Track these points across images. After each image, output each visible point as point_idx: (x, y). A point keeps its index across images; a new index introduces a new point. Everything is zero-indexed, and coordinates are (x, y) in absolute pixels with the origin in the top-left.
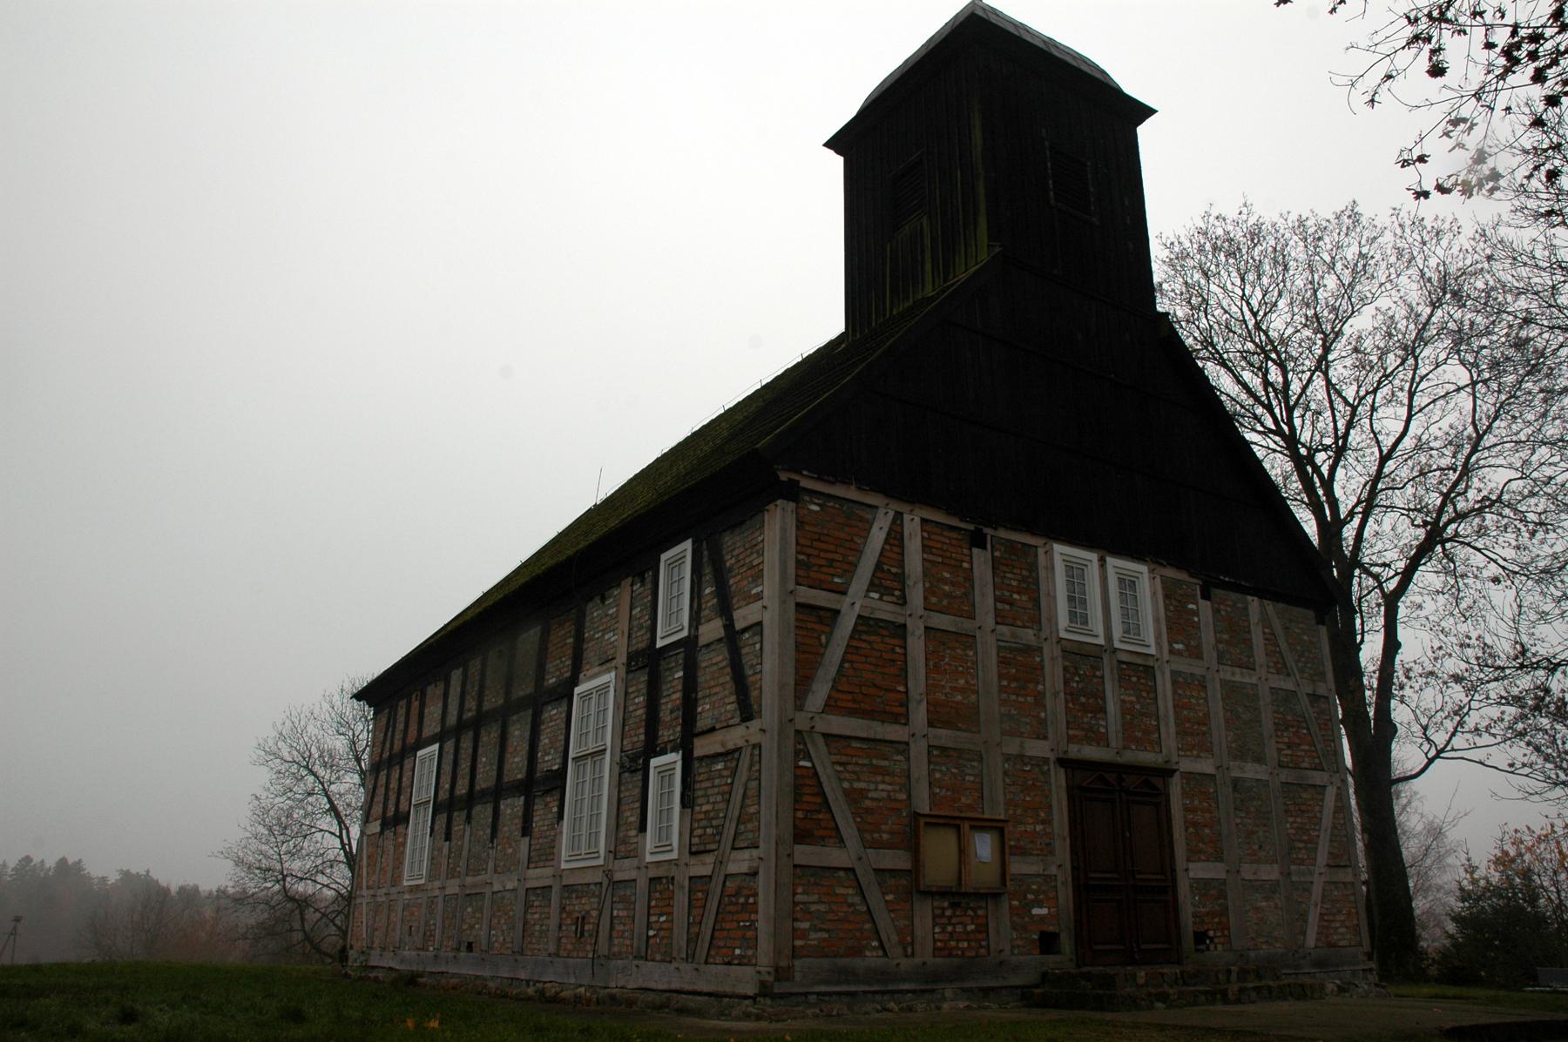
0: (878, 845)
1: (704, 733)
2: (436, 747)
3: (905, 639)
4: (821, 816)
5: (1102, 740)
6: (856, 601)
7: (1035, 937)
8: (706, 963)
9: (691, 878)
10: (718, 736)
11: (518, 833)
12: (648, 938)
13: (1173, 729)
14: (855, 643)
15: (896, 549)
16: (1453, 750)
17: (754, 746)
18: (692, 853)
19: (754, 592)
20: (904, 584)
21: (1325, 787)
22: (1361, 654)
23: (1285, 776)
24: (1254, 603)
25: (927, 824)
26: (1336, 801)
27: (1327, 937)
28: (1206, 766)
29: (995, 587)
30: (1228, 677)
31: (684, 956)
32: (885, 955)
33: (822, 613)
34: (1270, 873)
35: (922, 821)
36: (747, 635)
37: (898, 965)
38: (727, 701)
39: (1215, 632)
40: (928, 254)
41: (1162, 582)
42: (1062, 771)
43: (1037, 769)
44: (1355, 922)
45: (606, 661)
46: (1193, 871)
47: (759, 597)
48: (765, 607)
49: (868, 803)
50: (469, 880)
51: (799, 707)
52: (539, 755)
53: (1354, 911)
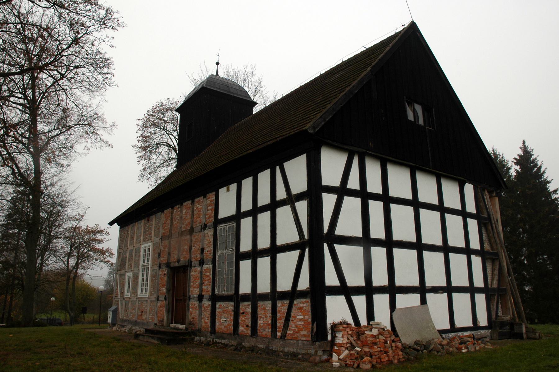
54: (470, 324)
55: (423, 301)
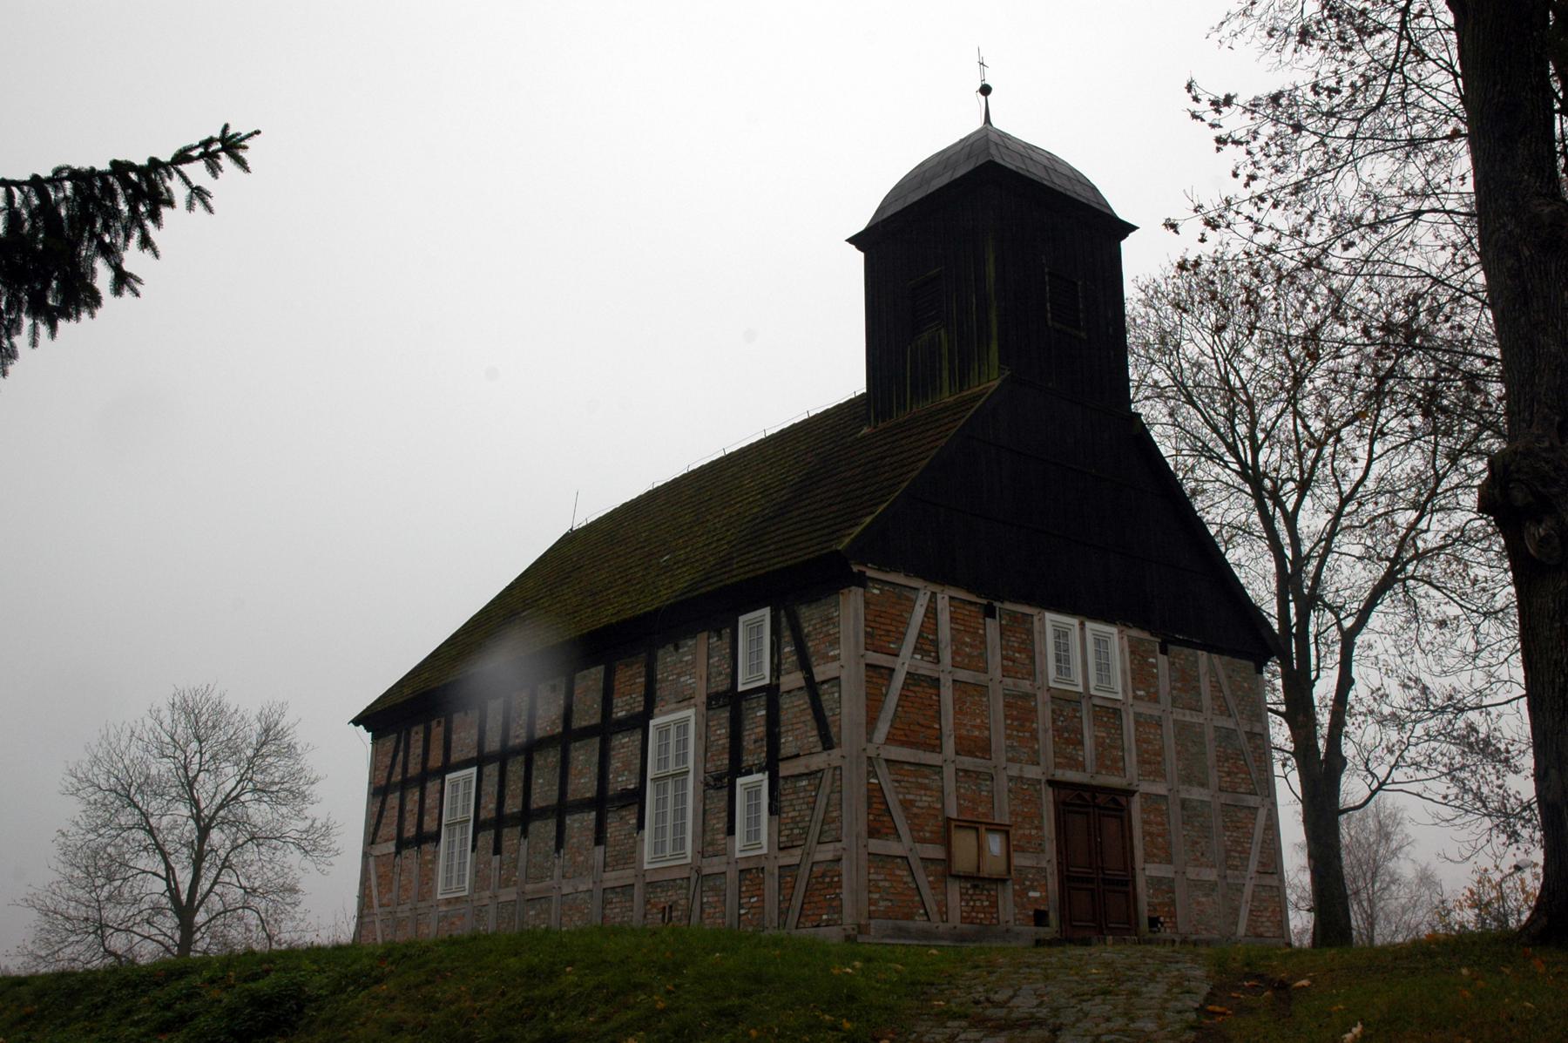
0: (923, 841)
1: (788, 758)
3: (939, 689)
4: (885, 819)
5: (1081, 766)
6: (906, 662)
7: (1031, 913)
8: (797, 928)
9: (780, 867)
10: (802, 761)
11: (590, 843)
12: (740, 915)
13: (1134, 758)
14: (905, 693)
15: (931, 621)
16: (1393, 782)
17: (835, 768)
18: (781, 849)
19: (832, 653)
20: (937, 646)
21: (1257, 808)
22: (1314, 690)
23: (1225, 798)
24: (1203, 656)
25: (956, 826)
26: (1267, 820)
27: (1254, 928)
28: (1160, 789)
29: (1002, 648)
30: (1180, 717)
31: (776, 925)
32: (929, 920)
33: (883, 671)
34: (1210, 875)
35: (953, 824)
36: (826, 686)
37: (937, 927)
38: (809, 734)
39: (1171, 681)
40: (945, 364)
41: (1129, 641)
42: (1050, 790)
43: (1032, 788)
44: (1279, 918)
45: (684, 700)
46: (1147, 871)
47: (836, 658)
48: (842, 666)
49: (915, 810)
50: (529, 887)
51: (870, 740)
52: (611, 776)
53: (1278, 909)
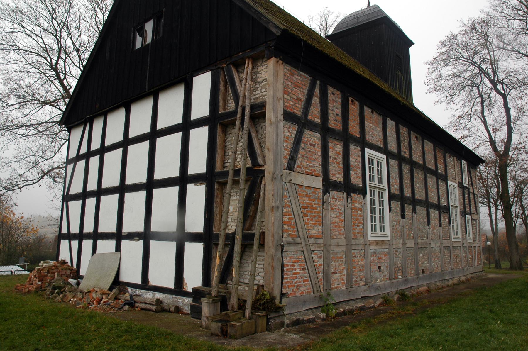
2: (318, 121)
54: (171, 285)
55: (118, 248)
